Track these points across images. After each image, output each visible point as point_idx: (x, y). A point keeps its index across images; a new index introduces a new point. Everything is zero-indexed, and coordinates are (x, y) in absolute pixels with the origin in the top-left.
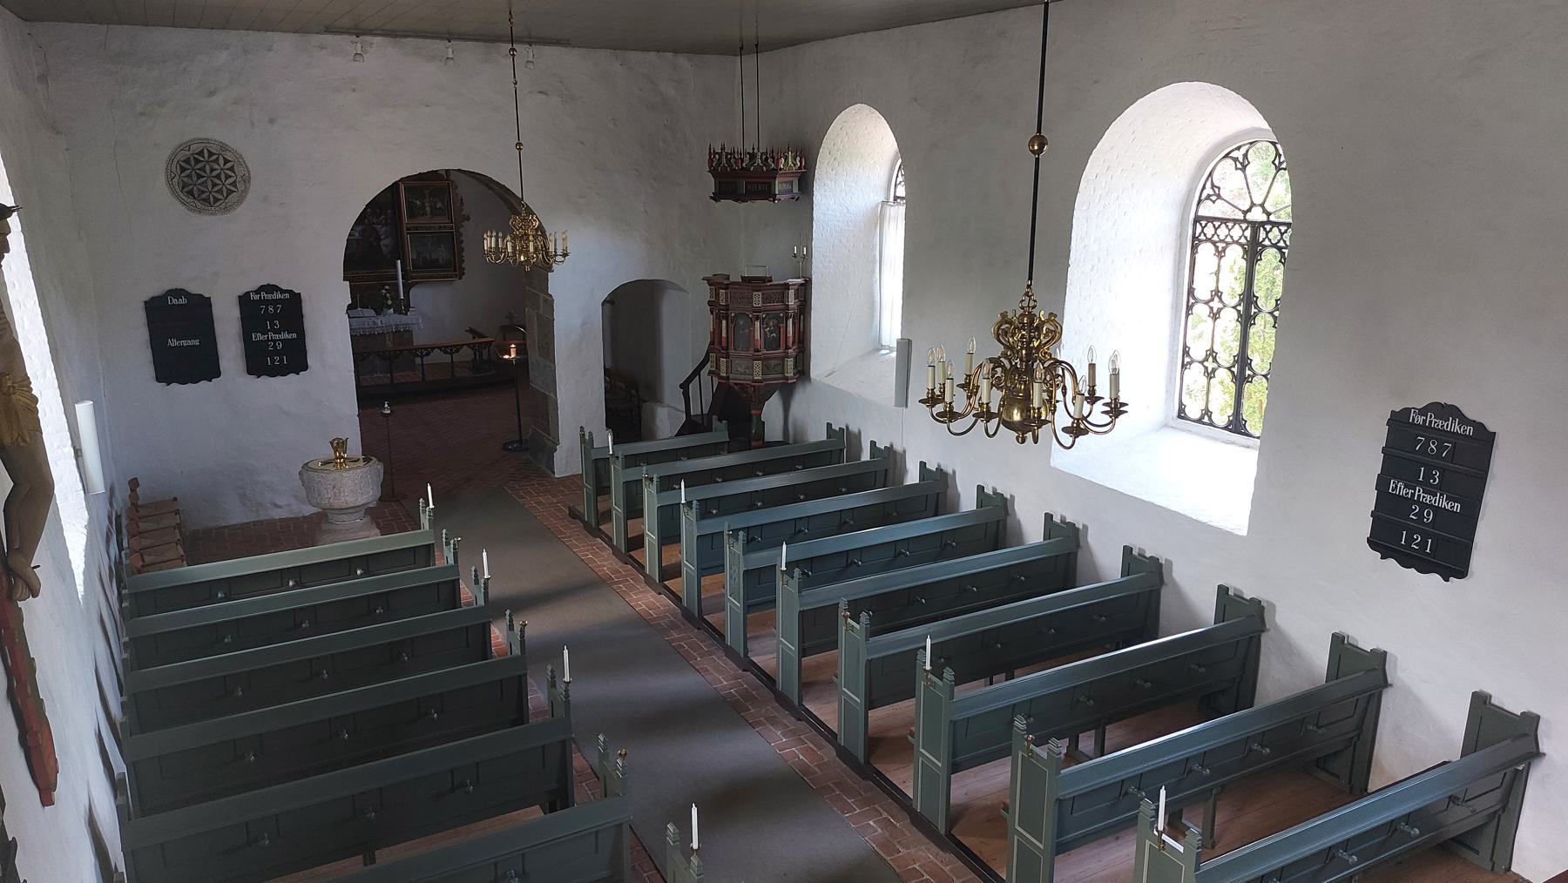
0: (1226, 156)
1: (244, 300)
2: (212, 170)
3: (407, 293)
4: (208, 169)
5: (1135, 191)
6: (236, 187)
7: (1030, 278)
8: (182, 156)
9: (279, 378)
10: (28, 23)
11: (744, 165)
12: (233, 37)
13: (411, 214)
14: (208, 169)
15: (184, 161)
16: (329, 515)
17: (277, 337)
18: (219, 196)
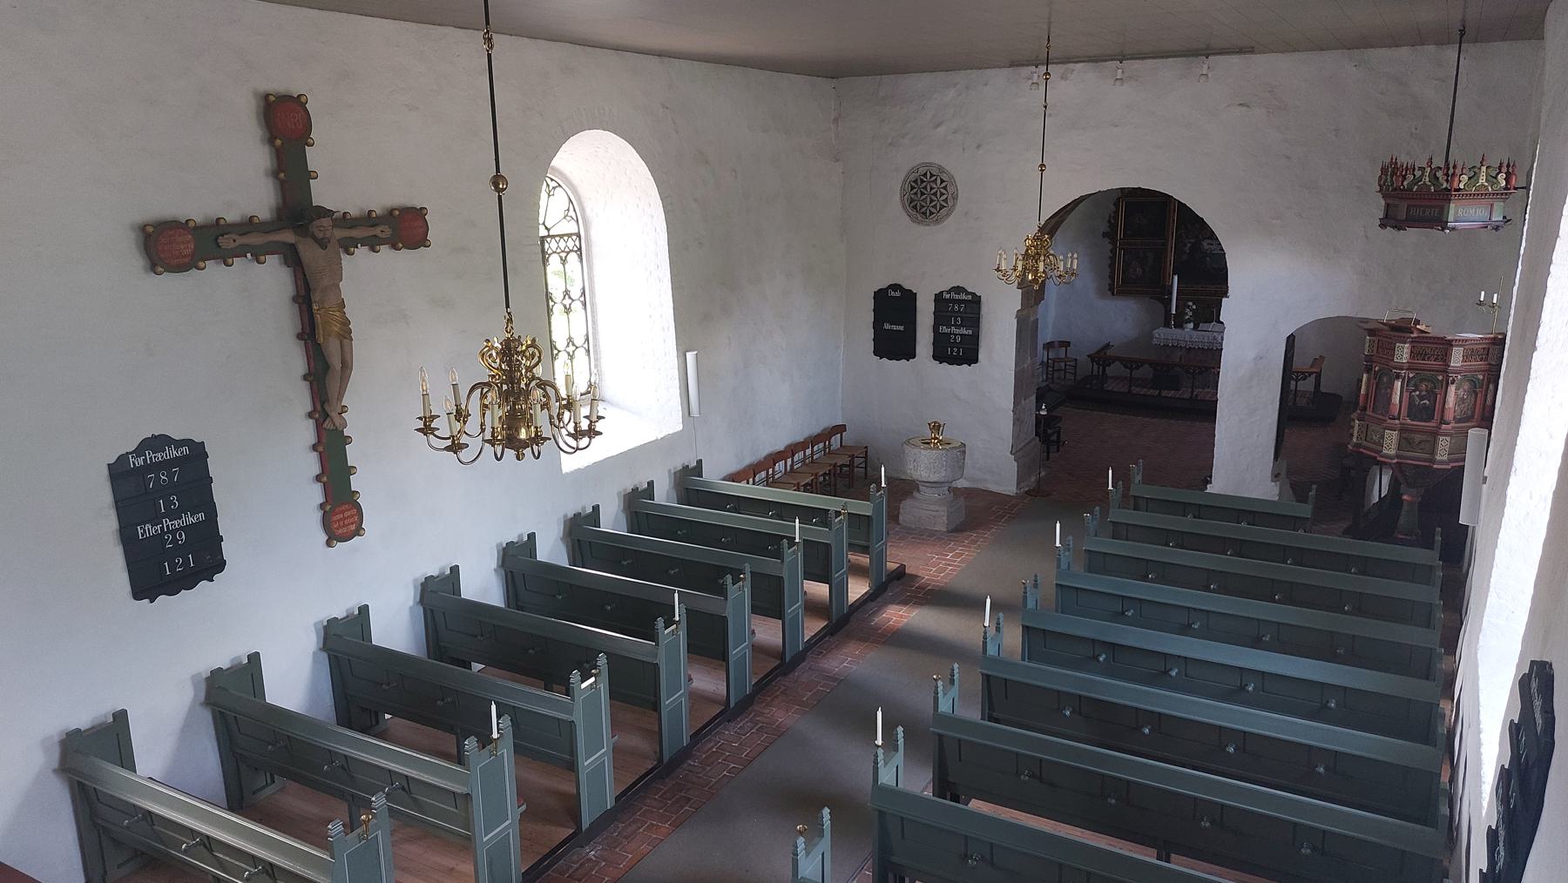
1: (939, 298)
2: (932, 188)
7: (508, 306)
8: (912, 178)
9: (955, 367)
11: (1405, 183)
12: (961, 77)
15: (914, 182)
16: (921, 487)
18: (933, 210)
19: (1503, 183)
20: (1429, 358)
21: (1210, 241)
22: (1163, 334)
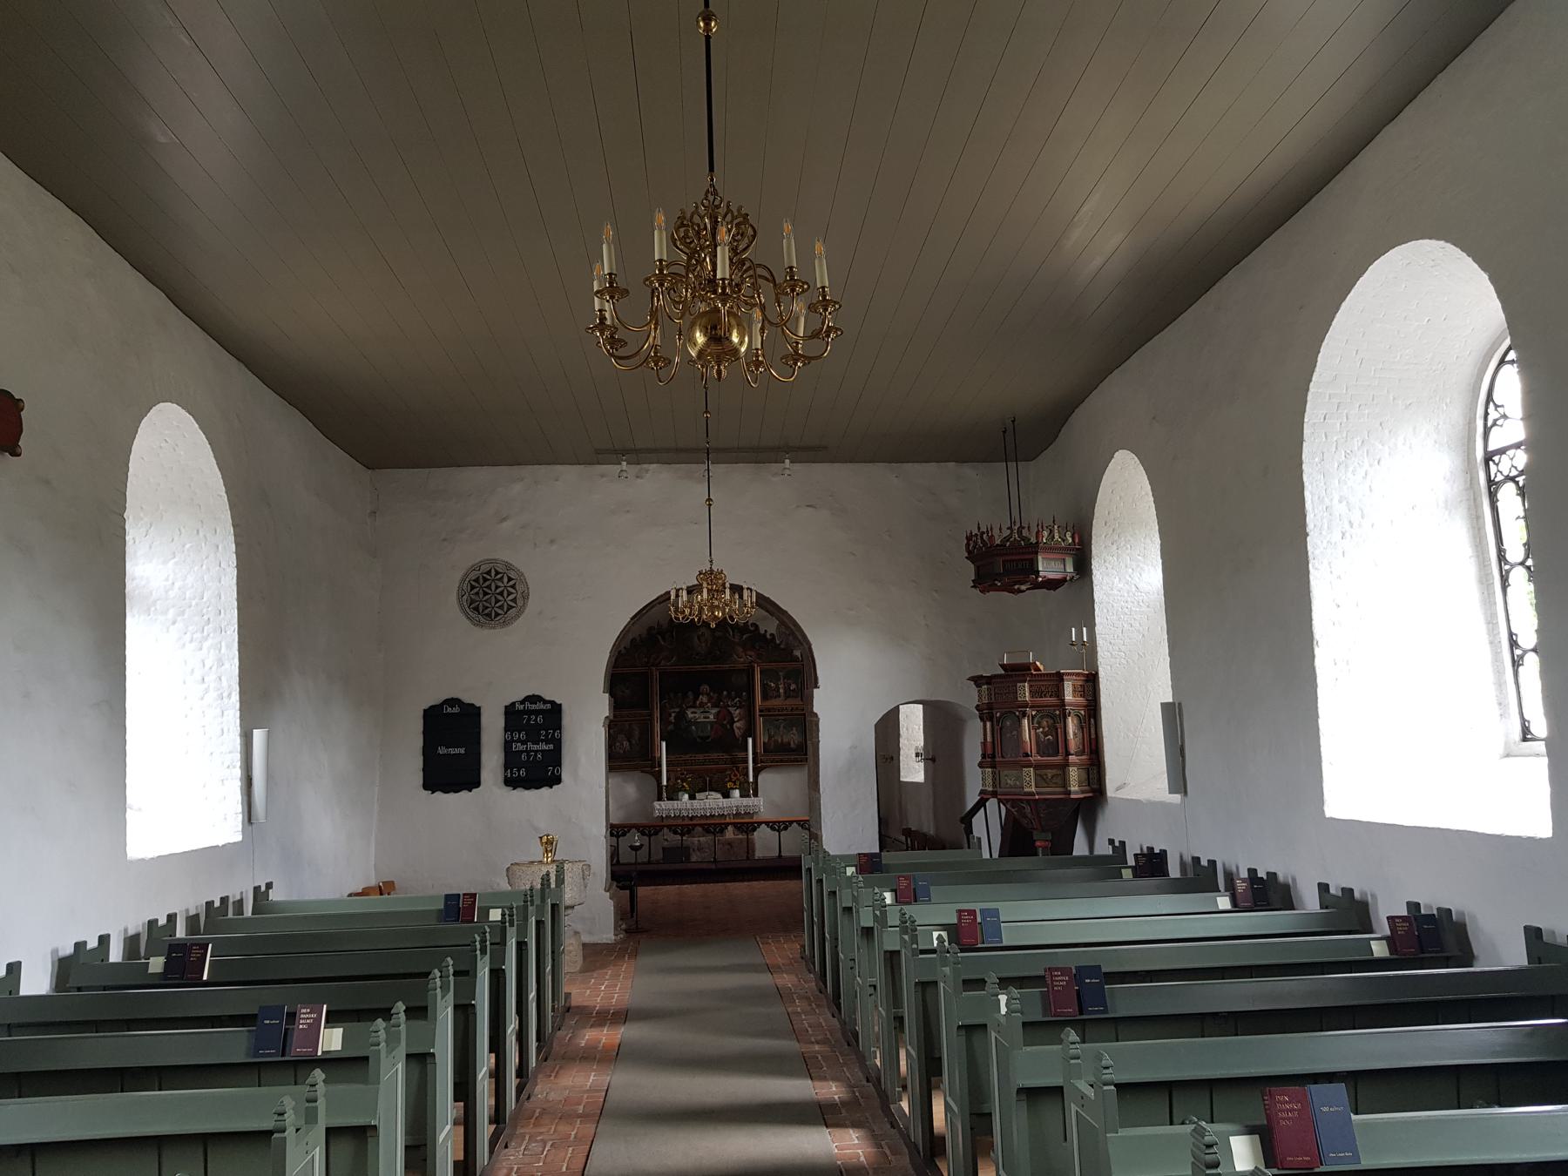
0: (1502, 362)
1: (511, 712)
2: (497, 587)
3: (756, 777)
4: (493, 588)
5: (1387, 431)
6: (516, 603)
8: (473, 576)
10: (370, 471)
13: (765, 697)
14: (493, 588)
15: (474, 581)
17: (535, 747)
18: (500, 611)
19: (1070, 540)
20: (1045, 695)
21: (693, 710)
22: (663, 807)
